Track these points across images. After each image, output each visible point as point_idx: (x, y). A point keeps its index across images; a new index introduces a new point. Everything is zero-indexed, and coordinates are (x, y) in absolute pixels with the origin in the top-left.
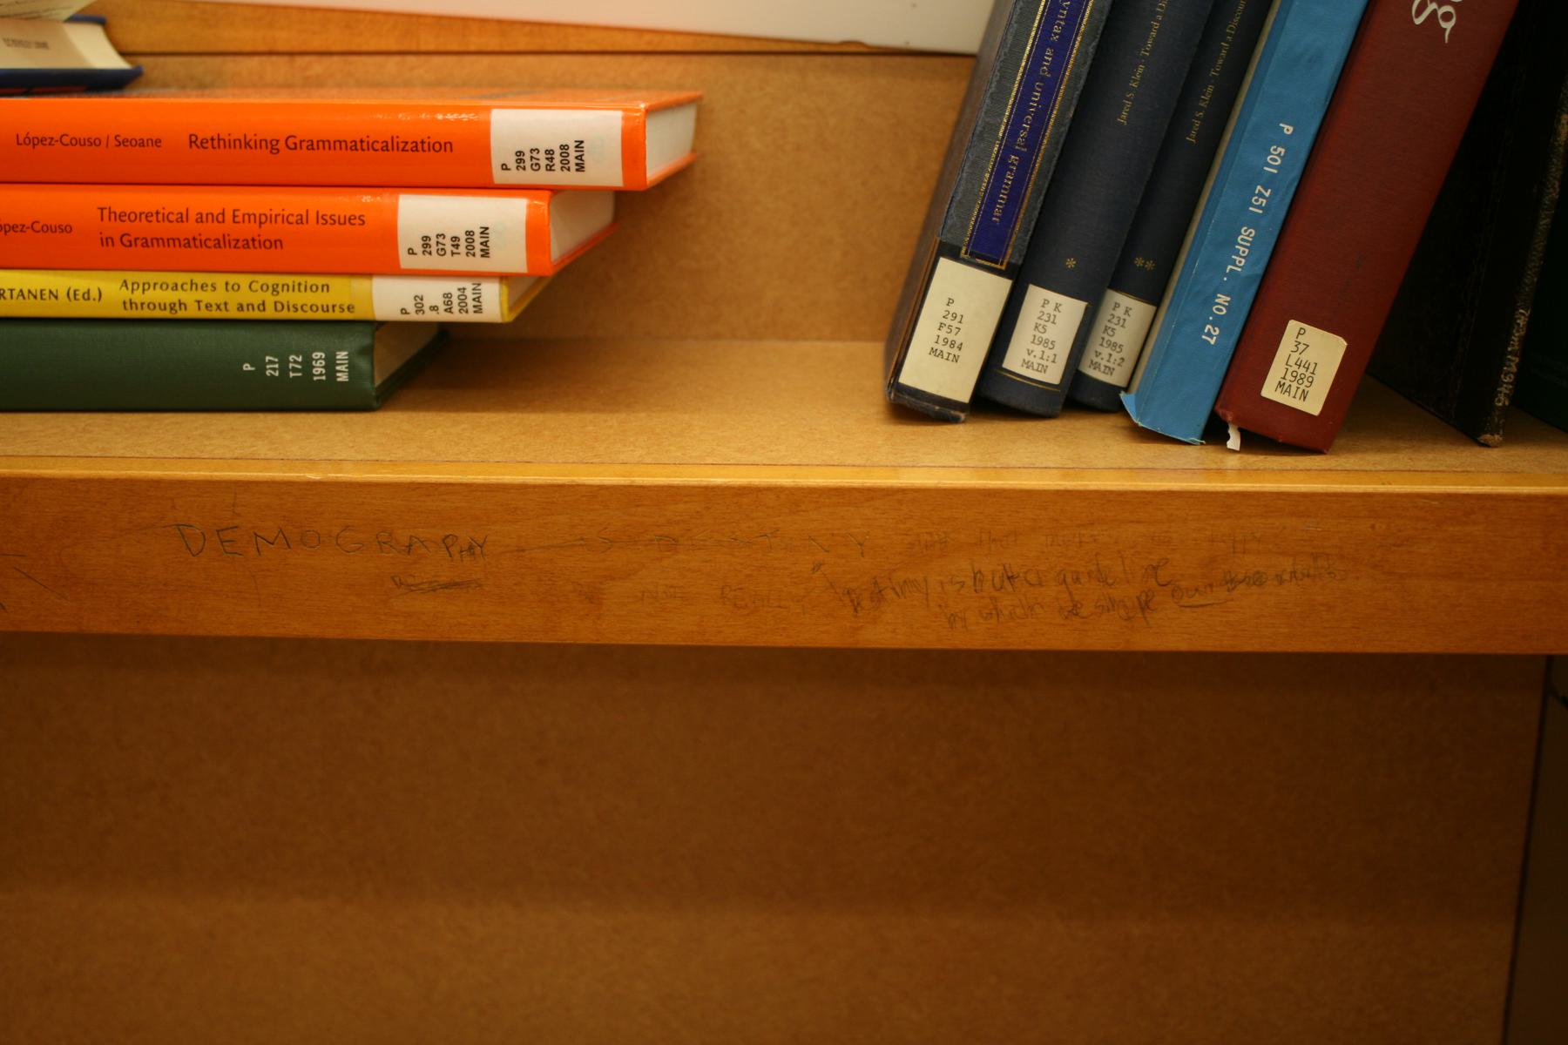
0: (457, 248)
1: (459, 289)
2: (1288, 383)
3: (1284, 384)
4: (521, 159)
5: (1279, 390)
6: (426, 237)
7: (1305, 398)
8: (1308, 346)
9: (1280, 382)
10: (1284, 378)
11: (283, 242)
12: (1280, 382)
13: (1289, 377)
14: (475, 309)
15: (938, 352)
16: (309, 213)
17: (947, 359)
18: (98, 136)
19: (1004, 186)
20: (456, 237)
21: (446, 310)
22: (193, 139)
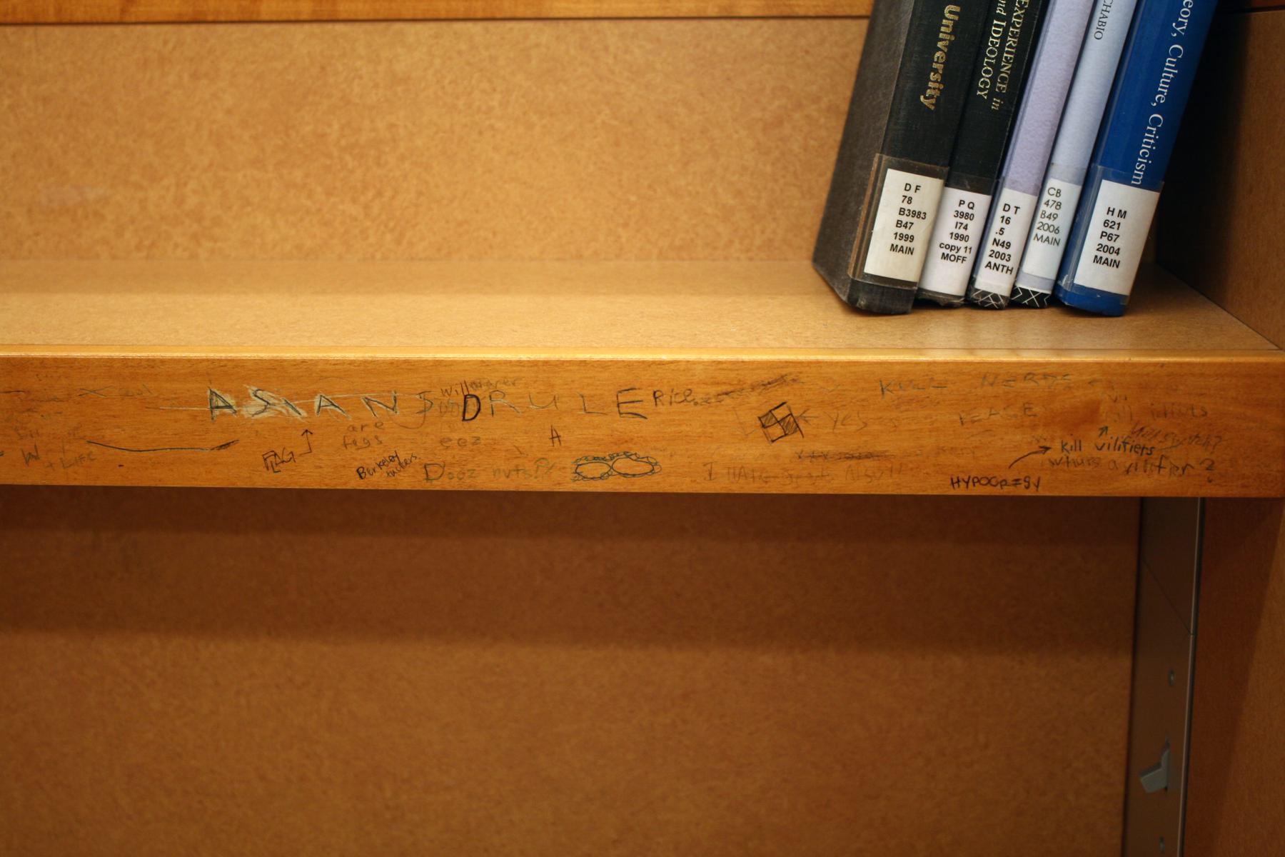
0: (1045, 204)
1: (1119, 249)
4: (902, 237)
14: (895, 246)
19: (1134, 177)
20: (1105, 223)
21: (990, 263)
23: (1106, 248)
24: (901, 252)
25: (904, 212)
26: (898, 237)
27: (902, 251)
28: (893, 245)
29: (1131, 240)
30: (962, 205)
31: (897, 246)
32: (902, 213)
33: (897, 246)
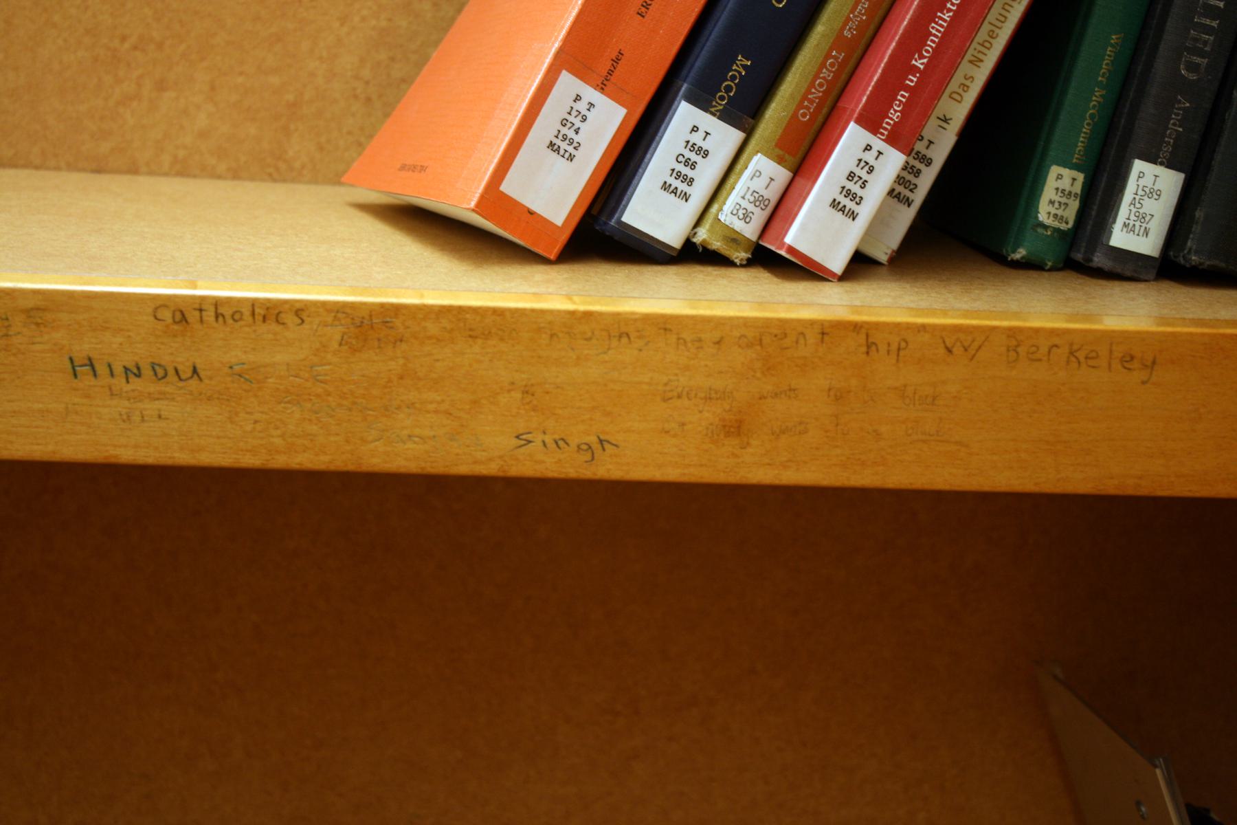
2: (1132, 223)
3: (1129, 224)
4: (679, 176)
5: (1125, 230)
6: (930, 164)
7: (1147, 235)
8: (1153, 216)
9: (1125, 223)
10: (1128, 219)
11: (756, 190)
12: (1125, 223)
13: (1132, 217)
14: (668, 184)
15: (556, 147)
16: (703, 138)
17: (563, 156)
18: (865, 189)
22: (690, 184)
23: (902, 180)
24: (841, 212)
25: (853, 177)
26: (674, 174)
27: (676, 194)
28: (835, 200)
29: (1160, 212)
30: (866, 151)
31: (670, 185)
32: (850, 178)
33: (670, 185)
